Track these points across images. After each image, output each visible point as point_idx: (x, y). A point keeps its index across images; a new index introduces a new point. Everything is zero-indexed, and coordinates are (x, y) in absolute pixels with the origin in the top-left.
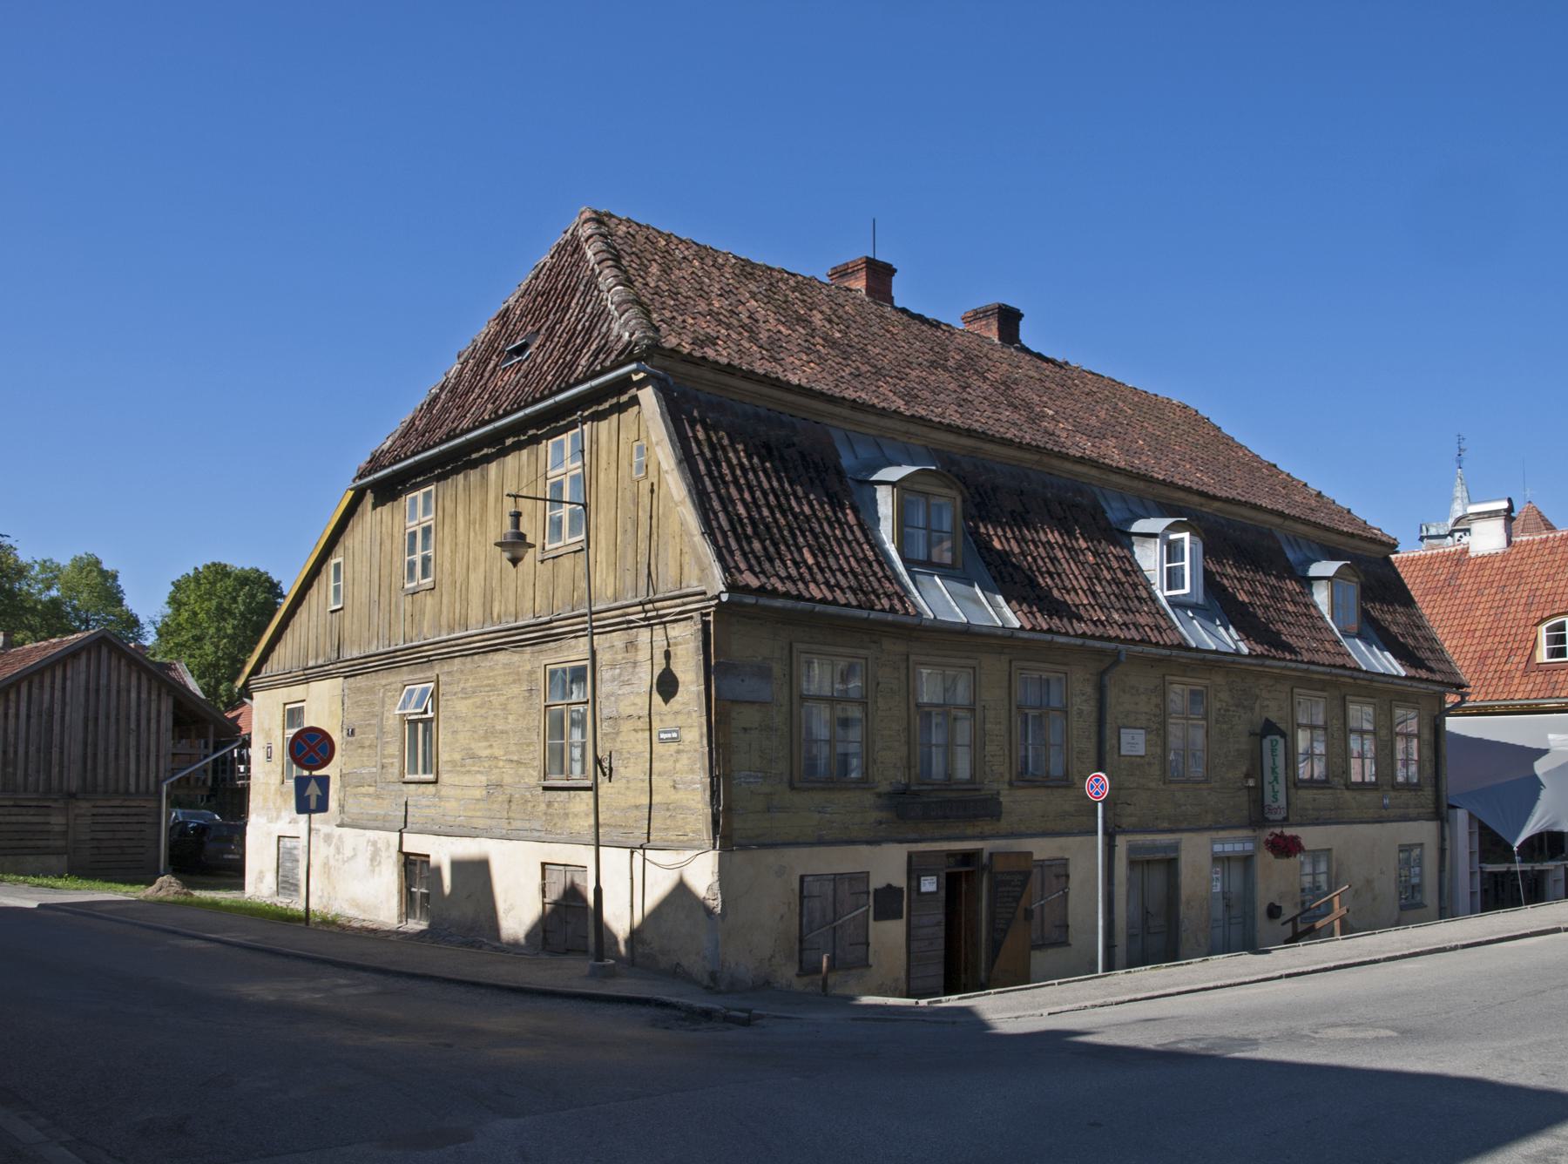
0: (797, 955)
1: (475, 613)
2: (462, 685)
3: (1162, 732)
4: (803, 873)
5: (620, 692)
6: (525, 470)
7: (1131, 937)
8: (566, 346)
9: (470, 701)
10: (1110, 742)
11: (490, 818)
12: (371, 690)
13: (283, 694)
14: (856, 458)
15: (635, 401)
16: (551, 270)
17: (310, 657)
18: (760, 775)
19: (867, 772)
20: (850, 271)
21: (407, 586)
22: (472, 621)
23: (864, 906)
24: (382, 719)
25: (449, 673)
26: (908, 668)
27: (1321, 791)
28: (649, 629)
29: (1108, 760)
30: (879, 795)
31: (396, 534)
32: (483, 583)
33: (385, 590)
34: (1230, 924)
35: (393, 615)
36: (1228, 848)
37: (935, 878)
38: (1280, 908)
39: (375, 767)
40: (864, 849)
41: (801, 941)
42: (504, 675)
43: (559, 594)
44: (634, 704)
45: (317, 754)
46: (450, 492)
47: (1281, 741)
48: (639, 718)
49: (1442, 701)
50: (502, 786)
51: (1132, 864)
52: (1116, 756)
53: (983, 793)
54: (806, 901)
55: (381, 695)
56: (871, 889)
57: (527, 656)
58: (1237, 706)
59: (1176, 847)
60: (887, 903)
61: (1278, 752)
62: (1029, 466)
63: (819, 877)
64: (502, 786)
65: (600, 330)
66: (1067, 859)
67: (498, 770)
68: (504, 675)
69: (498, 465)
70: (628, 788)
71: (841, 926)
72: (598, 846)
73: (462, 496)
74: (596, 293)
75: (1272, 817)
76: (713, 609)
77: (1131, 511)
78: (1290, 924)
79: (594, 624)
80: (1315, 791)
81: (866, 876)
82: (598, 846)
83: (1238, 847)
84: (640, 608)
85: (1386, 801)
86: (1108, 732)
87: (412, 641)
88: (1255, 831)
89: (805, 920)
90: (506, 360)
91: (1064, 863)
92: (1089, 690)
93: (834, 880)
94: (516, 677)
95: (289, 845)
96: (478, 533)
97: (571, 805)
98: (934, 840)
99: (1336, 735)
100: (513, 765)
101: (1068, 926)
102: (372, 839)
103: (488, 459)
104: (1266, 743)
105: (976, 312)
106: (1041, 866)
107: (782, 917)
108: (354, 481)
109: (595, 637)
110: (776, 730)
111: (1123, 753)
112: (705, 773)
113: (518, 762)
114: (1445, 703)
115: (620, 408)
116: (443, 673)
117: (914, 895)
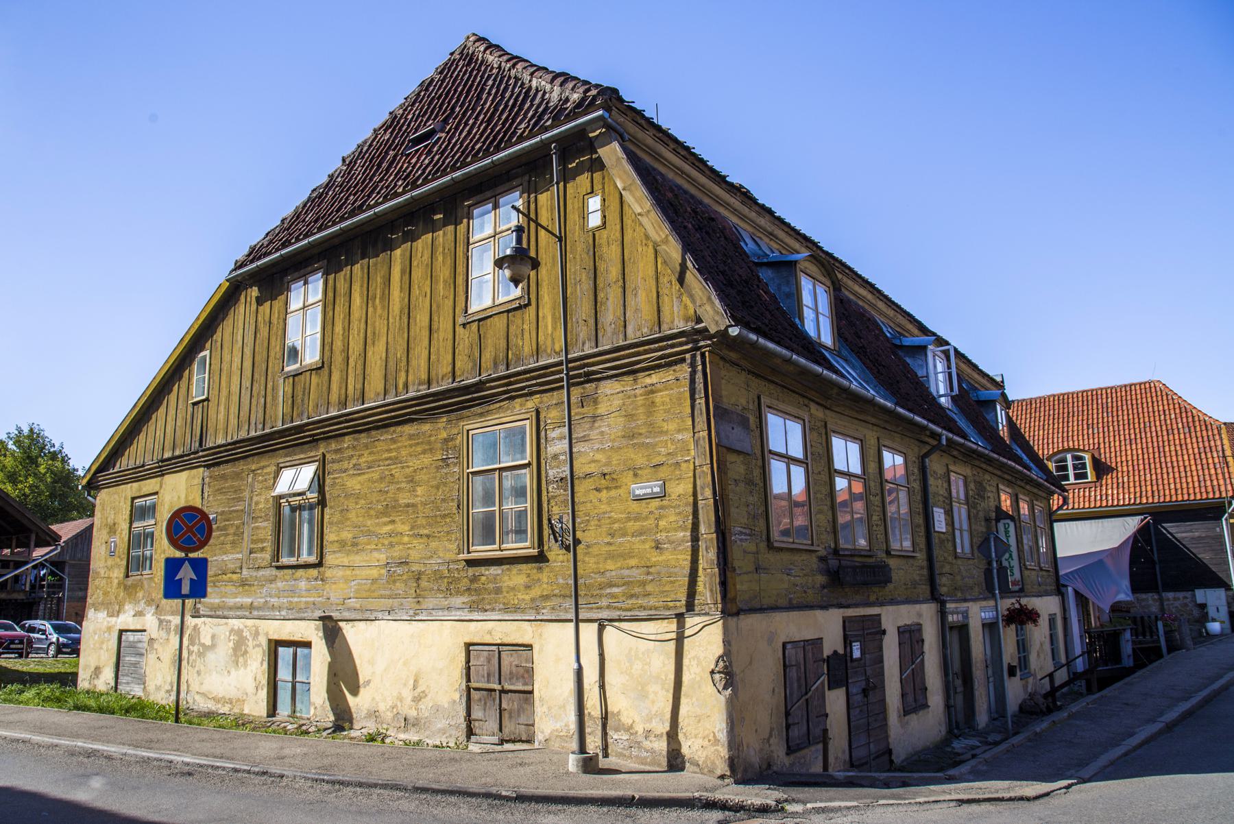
2: (354, 461)
11: (390, 597)
13: (130, 489)
17: (166, 449)
21: (287, 369)
22: (370, 394)
24: (250, 505)
25: (337, 451)
31: (275, 320)
32: (384, 355)
35: (269, 399)
40: (819, 613)
42: (411, 446)
45: (195, 535)
47: (1012, 525)
50: (406, 563)
54: (788, 670)
55: (250, 480)
61: (1010, 534)
64: (406, 563)
68: (411, 446)
71: (811, 696)
78: (1048, 678)
95: (131, 638)
96: (379, 307)
98: (856, 605)
101: (926, 689)
102: (236, 628)
104: (1001, 526)
113: (428, 536)
116: (328, 452)
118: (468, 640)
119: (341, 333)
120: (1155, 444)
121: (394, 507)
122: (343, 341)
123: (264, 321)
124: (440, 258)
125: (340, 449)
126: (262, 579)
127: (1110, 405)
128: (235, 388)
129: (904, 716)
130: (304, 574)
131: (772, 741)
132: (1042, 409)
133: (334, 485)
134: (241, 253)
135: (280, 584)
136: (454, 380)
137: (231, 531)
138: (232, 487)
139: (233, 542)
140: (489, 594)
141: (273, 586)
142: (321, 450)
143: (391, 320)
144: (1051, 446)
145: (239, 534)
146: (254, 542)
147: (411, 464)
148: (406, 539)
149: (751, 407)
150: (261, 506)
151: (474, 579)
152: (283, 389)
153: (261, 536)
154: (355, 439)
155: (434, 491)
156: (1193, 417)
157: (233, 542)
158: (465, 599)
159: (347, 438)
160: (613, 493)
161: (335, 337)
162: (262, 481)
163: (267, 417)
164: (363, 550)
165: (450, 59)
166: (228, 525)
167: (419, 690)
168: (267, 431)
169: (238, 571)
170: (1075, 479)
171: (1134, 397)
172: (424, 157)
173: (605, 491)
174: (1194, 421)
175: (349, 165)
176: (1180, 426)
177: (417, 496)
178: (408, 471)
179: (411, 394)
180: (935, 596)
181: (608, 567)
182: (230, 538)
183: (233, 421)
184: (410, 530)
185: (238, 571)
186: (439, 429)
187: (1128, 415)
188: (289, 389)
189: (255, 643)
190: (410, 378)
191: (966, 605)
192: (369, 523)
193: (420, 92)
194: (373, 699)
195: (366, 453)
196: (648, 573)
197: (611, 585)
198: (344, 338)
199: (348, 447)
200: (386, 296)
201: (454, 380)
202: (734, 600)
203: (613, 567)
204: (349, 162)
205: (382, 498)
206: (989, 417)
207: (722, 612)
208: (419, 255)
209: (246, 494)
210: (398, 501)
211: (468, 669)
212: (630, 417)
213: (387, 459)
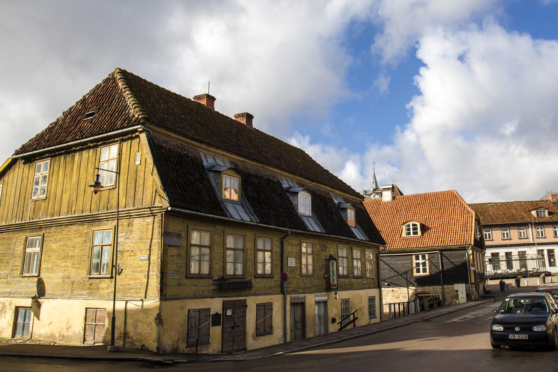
0: (186, 339)
1: (64, 209)
2: (54, 237)
3: (300, 259)
4: (189, 309)
5: (125, 242)
6: (91, 158)
7: (291, 330)
8: (111, 116)
9: (58, 244)
10: (285, 262)
11: (63, 290)
12: (9, 239)
14: (208, 162)
15: (138, 137)
16: (103, 88)
18: (176, 272)
19: (210, 272)
20: (201, 98)
22: (62, 213)
23: (208, 321)
24: (14, 251)
25: (49, 233)
26: (224, 235)
27: (346, 279)
28: (153, 217)
29: (284, 268)
30: (214, 280)
31: (30, 177)
32: (68, 198)
33: (22, 199)
34: (320, 325)
36: (320, 298)
37: (231, 310)
38: (335, 319)
39: (8, 270)
40: (209, 300)
41: (188, 334)
42: (75, 234)
43: (102, 204)
44: (130, 246)
46: (57, 163)
47: (335, 262)
48: (132, 251)
49: (379, 249)
50: (69, 278)
51: (292, 304)
52: (286, 267)
53: (246, 279)
54: (190, 319)
55: (15, 241)
56: (211, 314)
57: (86, 226)
58: (322, 250)
59: (305, 298)
60: (216, 319)
62: (259, 168)
63: (195, 310)
64: (69, 278)
65: (125, 112)
66: (272, 303)
67: (68, 271)
68: (75, 234)
69: (79, 155)
70: (125, 278)
71: (201, 328)
72: (114, 300)
73: (63, 165)
74: (123, 98)
75: (333, 288)
76: (164, 213)
77: (289, 184)
79: (119, 216)
80: (344, 279)
81: (209, 309)
82: (114, 300)
83: (323, 298)
84: (149, 209)
85: (364, 282)
86: (284, 259)
87: (33, 219)
88: (327, 292)
89: (189, 326)
90: (84, 118)
91: (271, 304)
92: (278, 244)
93: (199, 311)
94: (80, 235)
97: (101, 285)
99: (350, 260)
100: (76, 269)
102: (2, 302)
103: (75, 151)
105: (239, 115)
106: (264, 305)
107: (182, 325)
108: (13, 155)
109: (119, 220)
110: (182, 256)
111: (289, 266)
112: (159, 272)
113: (77, 268)
114: (380, 250)
115: (132, 138)
116: (46, 233)
117: (225, 316)
118: (87, 307)
119: (54, 187)
120: (448, 220)
121: (67, 256)
122: (54, 190)
123: (26, 177)
124: (90, 165)
125: (50, 232)
126: (16, 281)
127: (434, 200)
128: (12, 202)
129: (256, 337)
130: (32, 280)
131: (179, 342)
132: (408, 201)
133: (46, 246)
134: (19, 147)
135: (22, 284)
136: (90, 212)
137: (5, 261)
138: (7, 243)
139: (5, 266)
140: (95, 290)
141: (20, 284)
142: (43, 232)
143: (72, 185)
144: (407, 219)
145: (8, 262)
146: (14, 266)
147: (74, 241)
148: (70, 269)
149: (183, 230)
150: (18, 252)
151: (91, 284)
152: (31, 205)
153: (17, 264)
154: (56, 229)
155: (81, 251)
156: (464, 208)
157: (5, 266)
158: (87, 291)
159: (53, 228)
160: (135, 257)
161: (52, 188)
162: (19, 242)
163: (23, 216)
164: (55, 272)
165: (108, 77)
166: (4, 259)
167: (69, 325)
168: (23, 222)
169: (6, 278)
170: (413, 235)
171: (444, 197)
172: (89, 124)
173: (132, 257)
174: (464, 210)
175: (65, 116)
176: (459, 211)
177: (75, 253)
178: (73, 243)
179: (76, 215)
180: (282, 292)
181: (131, 283)
182: (4, 264)
183: (10, 216)
184: (72, 265)
185: (6, 278)
186: (84, 229)
187: (440, 205)
188: (33, 206)
189: (10, 307)
190: (77, 209)
191: (305, 295)
192: (58, 261)
193: (96, 89)
194: (53, 329)
195: (59, 235)
196: (142, 285)
197: (131, 289)
198: (55, 189)
199: (53, 232)
200: (71, 176)
201: (90, 212)
202: (165, 295)
203: (132, 283)
204: (66, 114)
205: (63, 252)
206: (343, 215)
207: (160, 299)
208: (84, 162)
209: (12, 246)
210: (68, 254)
211: (86, 317)
212: (142, 232)
213: (66, 238)
